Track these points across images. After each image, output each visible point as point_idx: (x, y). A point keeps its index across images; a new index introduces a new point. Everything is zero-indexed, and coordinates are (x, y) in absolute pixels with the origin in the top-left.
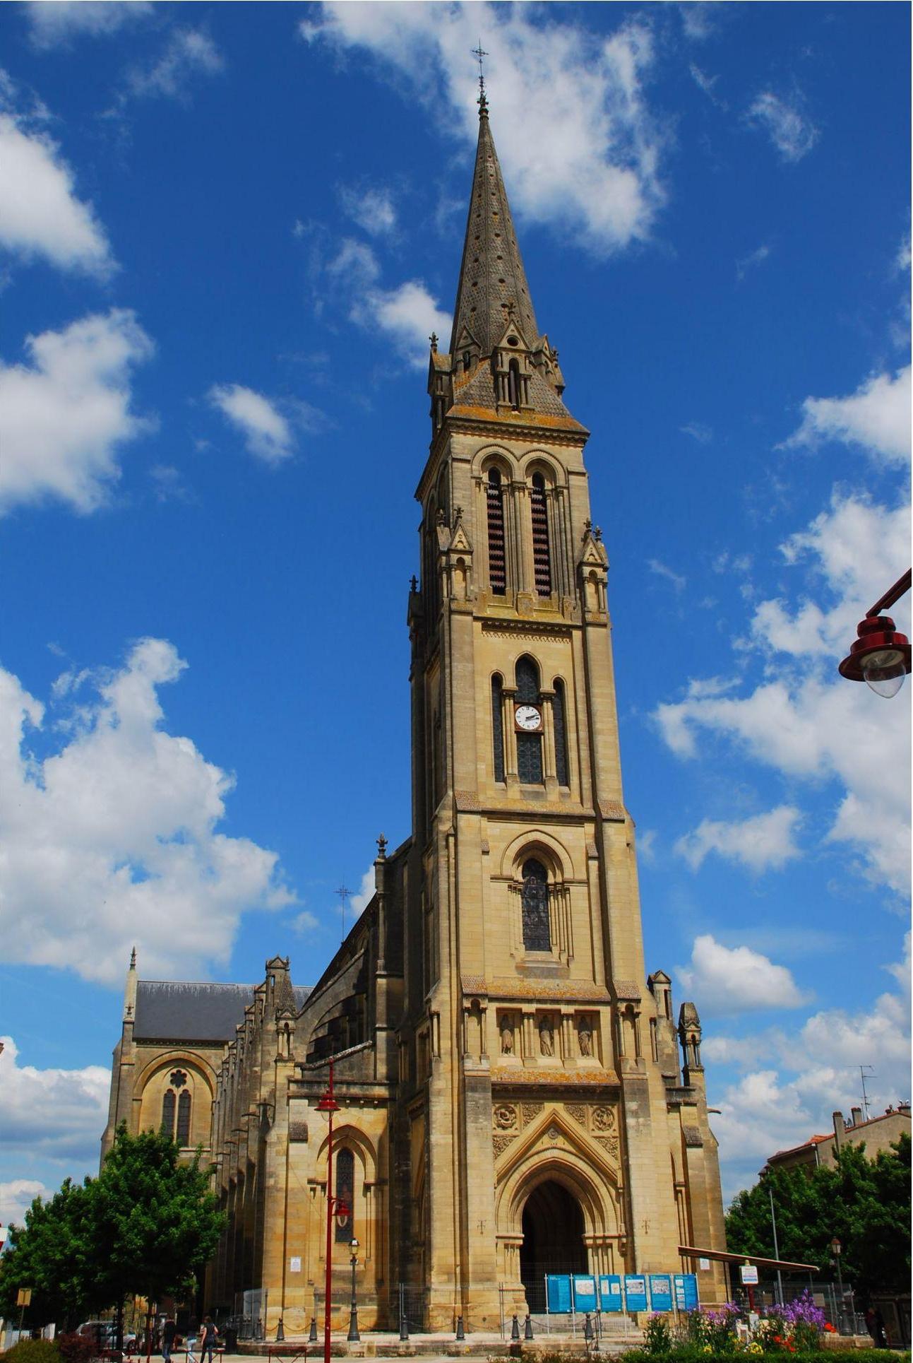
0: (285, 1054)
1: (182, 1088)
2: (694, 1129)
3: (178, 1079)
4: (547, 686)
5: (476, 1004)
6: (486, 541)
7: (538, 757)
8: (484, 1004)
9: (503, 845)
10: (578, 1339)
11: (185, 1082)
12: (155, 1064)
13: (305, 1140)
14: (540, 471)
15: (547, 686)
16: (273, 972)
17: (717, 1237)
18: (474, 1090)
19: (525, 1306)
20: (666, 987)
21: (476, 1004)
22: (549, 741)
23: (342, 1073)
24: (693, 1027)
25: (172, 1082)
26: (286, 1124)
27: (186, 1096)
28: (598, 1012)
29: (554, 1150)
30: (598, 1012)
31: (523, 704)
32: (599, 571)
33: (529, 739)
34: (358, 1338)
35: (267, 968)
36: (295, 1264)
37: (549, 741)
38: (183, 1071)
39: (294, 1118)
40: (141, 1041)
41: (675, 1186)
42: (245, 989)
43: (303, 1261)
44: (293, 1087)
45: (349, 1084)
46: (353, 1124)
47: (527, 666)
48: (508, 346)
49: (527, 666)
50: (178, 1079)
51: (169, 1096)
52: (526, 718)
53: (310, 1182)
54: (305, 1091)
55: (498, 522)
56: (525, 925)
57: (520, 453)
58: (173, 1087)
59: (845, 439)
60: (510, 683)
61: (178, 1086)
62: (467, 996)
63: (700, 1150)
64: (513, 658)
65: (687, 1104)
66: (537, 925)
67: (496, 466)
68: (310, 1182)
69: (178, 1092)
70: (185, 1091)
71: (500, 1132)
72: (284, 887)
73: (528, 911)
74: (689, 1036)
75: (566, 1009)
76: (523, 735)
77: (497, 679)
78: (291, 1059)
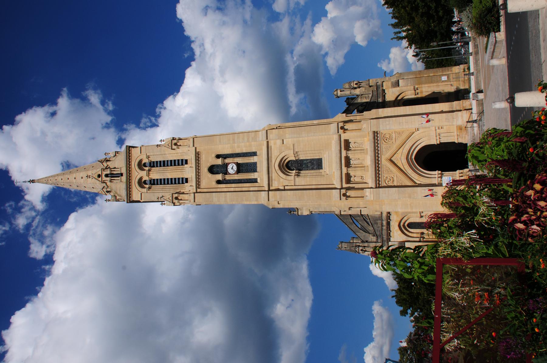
2: (392, 83)
4: (219, 162)
7: (247, 164)
9: (281, 180)
15: (219, 162)
17: (434, 72)
18: (379, 184)
20: (339, 91)
22: (240, 160)
23: (378, 227)
29: (401, 160)
31: (227, 170)
33: (241, 168)
37: (240, 160)
41: (376, 188)
46: (397, 224)
47: (212, 170)
48: (96, 177)
49: (212, 170)
52: (232, 169)
56: (313, 169)
57: (137, 174)
59: (23, 113)
60: (219, 177)
63: (400, 81)
64: (210, 175)
65: (382, 87)
66: (313, 164)
72: (405, 43)
73: (307, 168)
74: (355, 86)
76: (238, 171)
77: (219, 182)
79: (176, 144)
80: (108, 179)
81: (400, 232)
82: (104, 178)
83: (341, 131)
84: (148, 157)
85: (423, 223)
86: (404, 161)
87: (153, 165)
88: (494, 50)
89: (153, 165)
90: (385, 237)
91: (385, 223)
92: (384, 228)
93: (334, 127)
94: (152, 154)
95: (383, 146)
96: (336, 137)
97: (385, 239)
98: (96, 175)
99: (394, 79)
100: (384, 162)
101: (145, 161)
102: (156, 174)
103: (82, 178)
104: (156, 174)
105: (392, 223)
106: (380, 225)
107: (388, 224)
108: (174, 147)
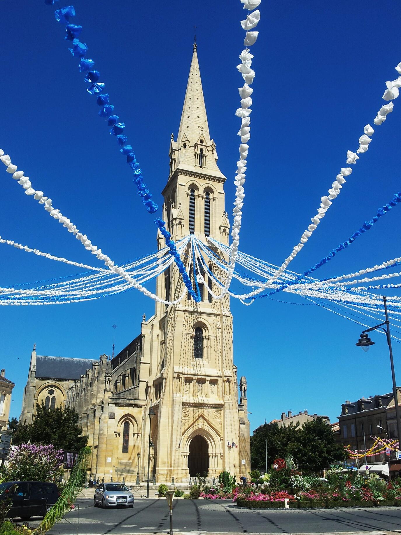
0: (108, 389)
1: (53, 395)
3: (51, 392)
5: (178, 376)
6: (189, 215)
8: (181, 375)
10: (369, 466)
11: (54, 393)
12: (43, 387)
13: (114, 418)
14: (208, 191)
16: (103, 359)
19: (189, 475)
21: (178, 376)
23: (127, 395)
24: (244, 385)
25: (49, 393)
26: (107, 413)
27: (54, 399)
28: (217, 380)
29: (201, 424)
30: (217, 380)
32: (227, 229)
34: (139, 484)
35: (100, 358)
36: (109, 460)
38: (53, 389)
39: (110, 411)
40: (38, 378)
42: (76, 360)
43: (112, 459)
44: (110, 400)
45: (130, 399)
46: (130, 413)
48: (201, 138)
50: (51, 392)
51: (48, 398)
53: (115, 432)
54: (114, 402)
55: (208, 226)
57: (202, 184)
58: (49, 395)
61: (51, 395)
62: (175, 373)
65: (241, 410)
67: (193, 188)
68: (115, 432)
69: (51, 397)
70: (54, 397)
71: (184, 418)
74: (243, 387)
75: (208, 378)
78: (110, 391)
79: (224, 230)
80: (199, 152)
81: (123, 415)
82: (199, 147)
83: (226, 379)
84: (214, 199)
85: (128, 436)
86: (200, 426)
87: (207, 201)
88: (128, 518)
89: (207, 201)
90: (120, 401)
91: (132, 402)
92: (128, 401)
93: (229, 372)
94: (217, 204)
95: (212, 411)
96: (220, 374)
97: (118, 401)
98: (203, 139)
99: (246, 420)
100: (201, 411)
101: (211, 196)
102: (200, 204)
103: (198, 117)
104: (200, 204)
105: (131, 408)
106: (129, 397)
107: (131, 405)
108: (222, 229)
